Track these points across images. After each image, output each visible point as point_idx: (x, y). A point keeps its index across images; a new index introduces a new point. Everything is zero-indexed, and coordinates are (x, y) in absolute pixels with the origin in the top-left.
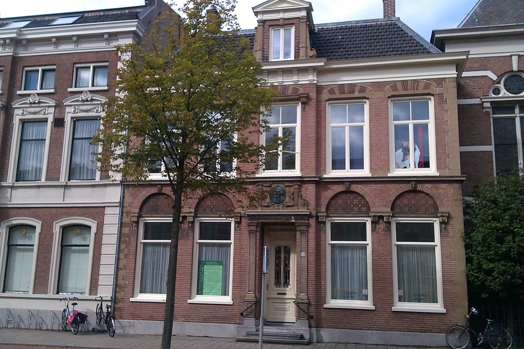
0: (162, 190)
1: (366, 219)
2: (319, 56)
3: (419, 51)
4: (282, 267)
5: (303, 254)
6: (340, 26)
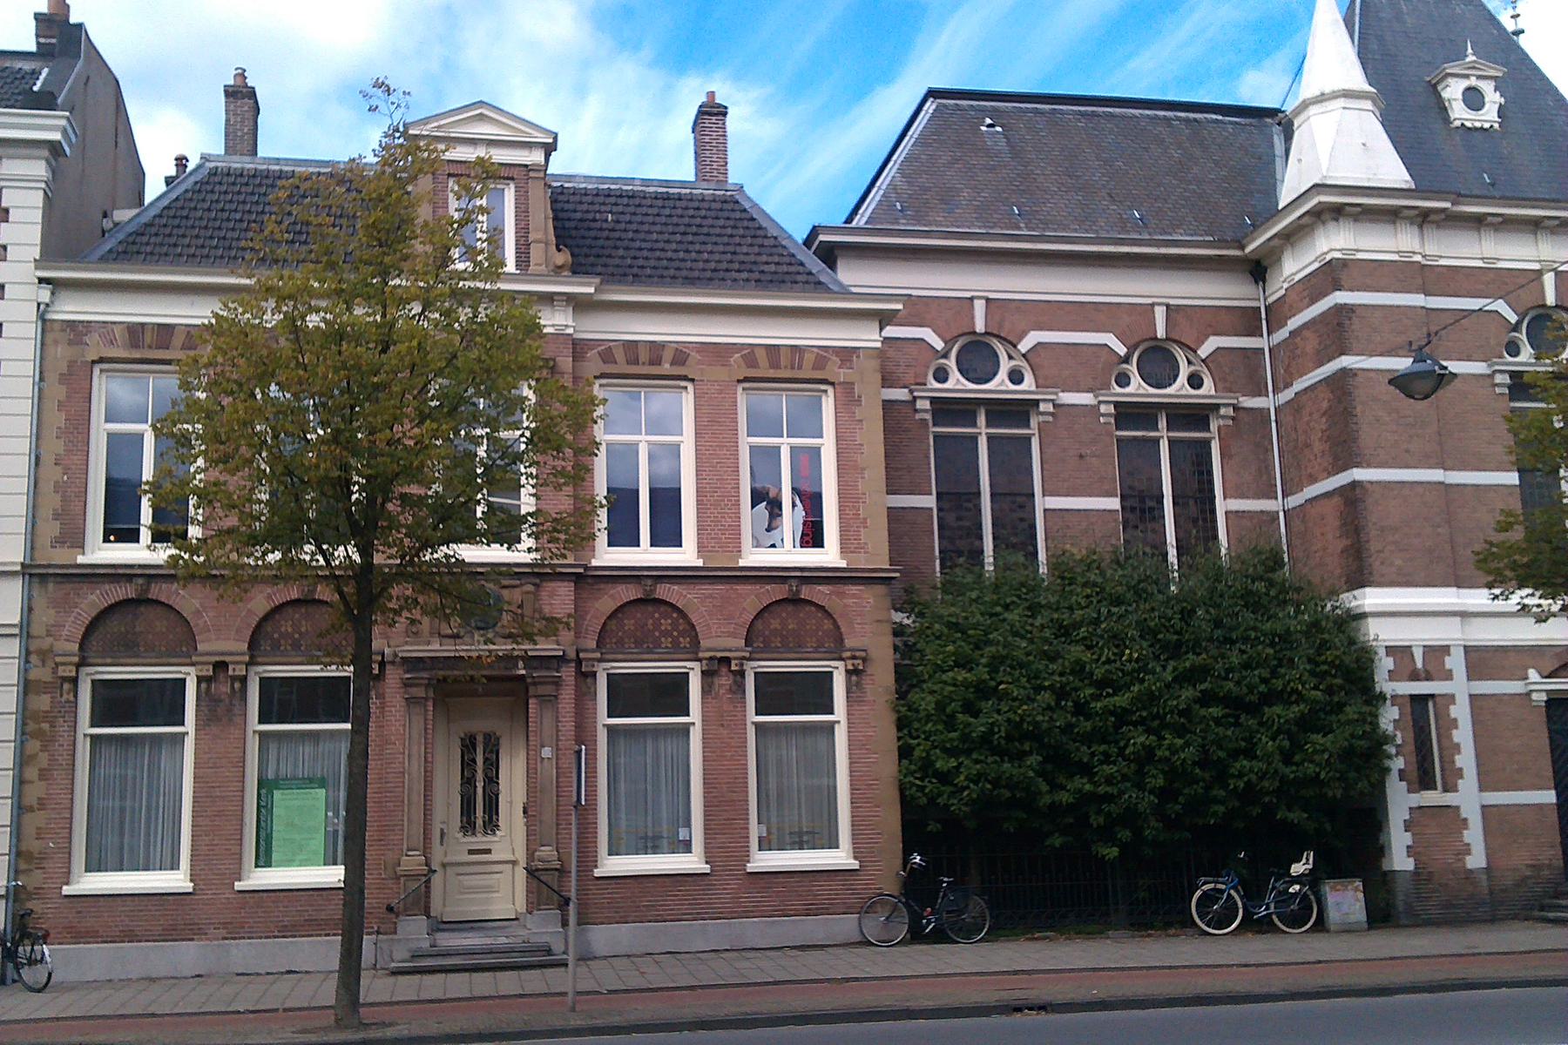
0: (147, 591)
2: (578, 269)
4: (480, 785)
5: (547, 752)
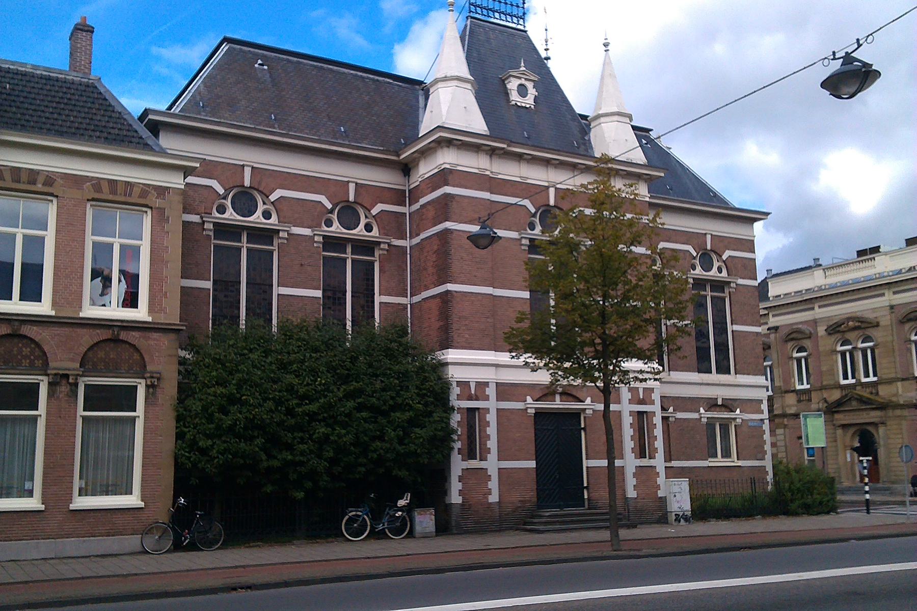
1: (40, 377)
3: (133, 140)
6: (7, 66)
